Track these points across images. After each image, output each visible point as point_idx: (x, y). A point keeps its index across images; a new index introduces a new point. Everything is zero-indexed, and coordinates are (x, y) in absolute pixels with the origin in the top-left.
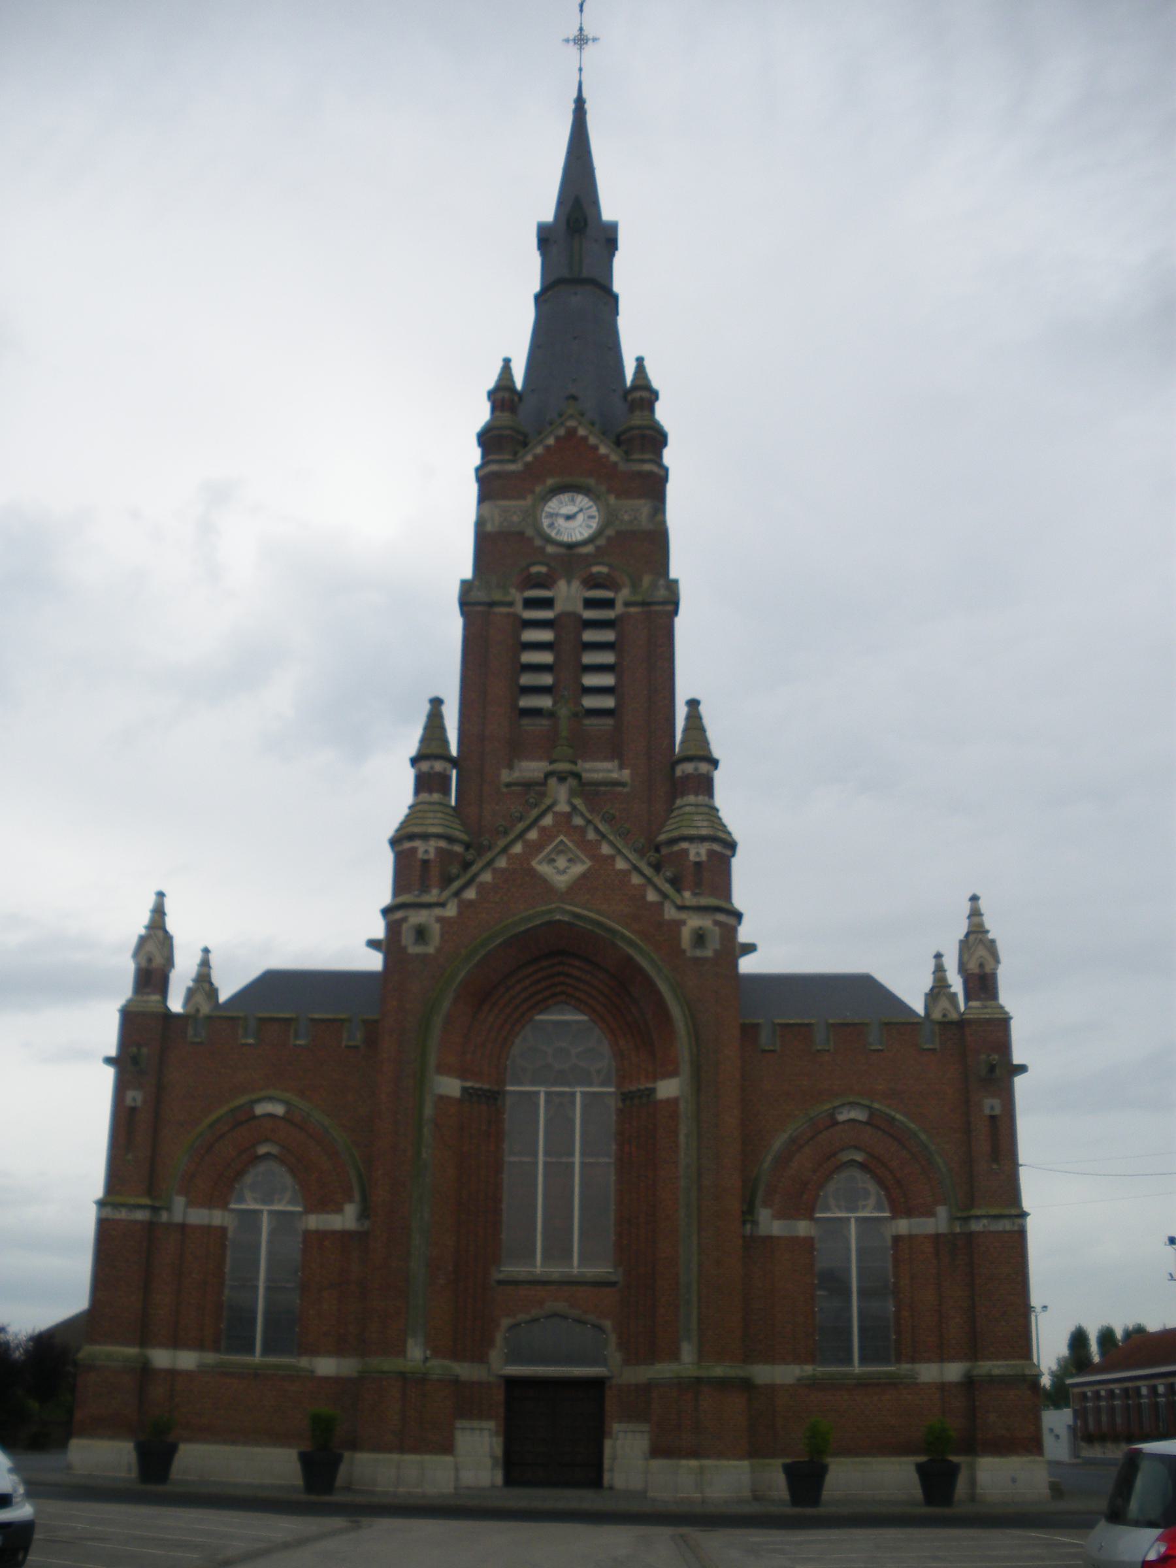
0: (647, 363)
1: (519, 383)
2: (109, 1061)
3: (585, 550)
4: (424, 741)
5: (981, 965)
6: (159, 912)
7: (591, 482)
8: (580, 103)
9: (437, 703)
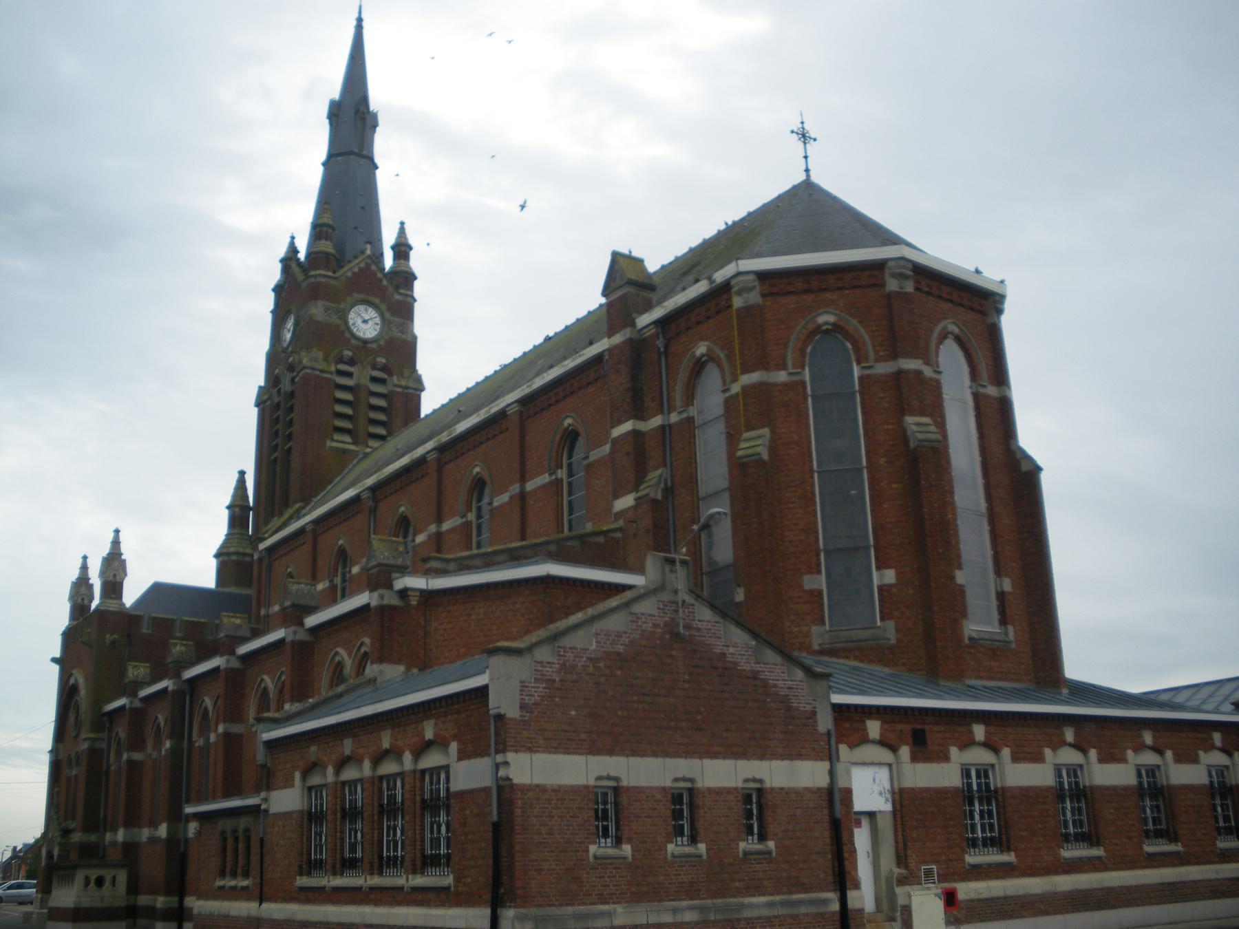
0: (406, 226)
1: (302, 256)
2: (54, 660)
3: (374, 346)
4: (235, 496)
5: (115, 576)
6: (116, 543)
7: (377, 301)
8: (360, 20)
9: (242, 473)
